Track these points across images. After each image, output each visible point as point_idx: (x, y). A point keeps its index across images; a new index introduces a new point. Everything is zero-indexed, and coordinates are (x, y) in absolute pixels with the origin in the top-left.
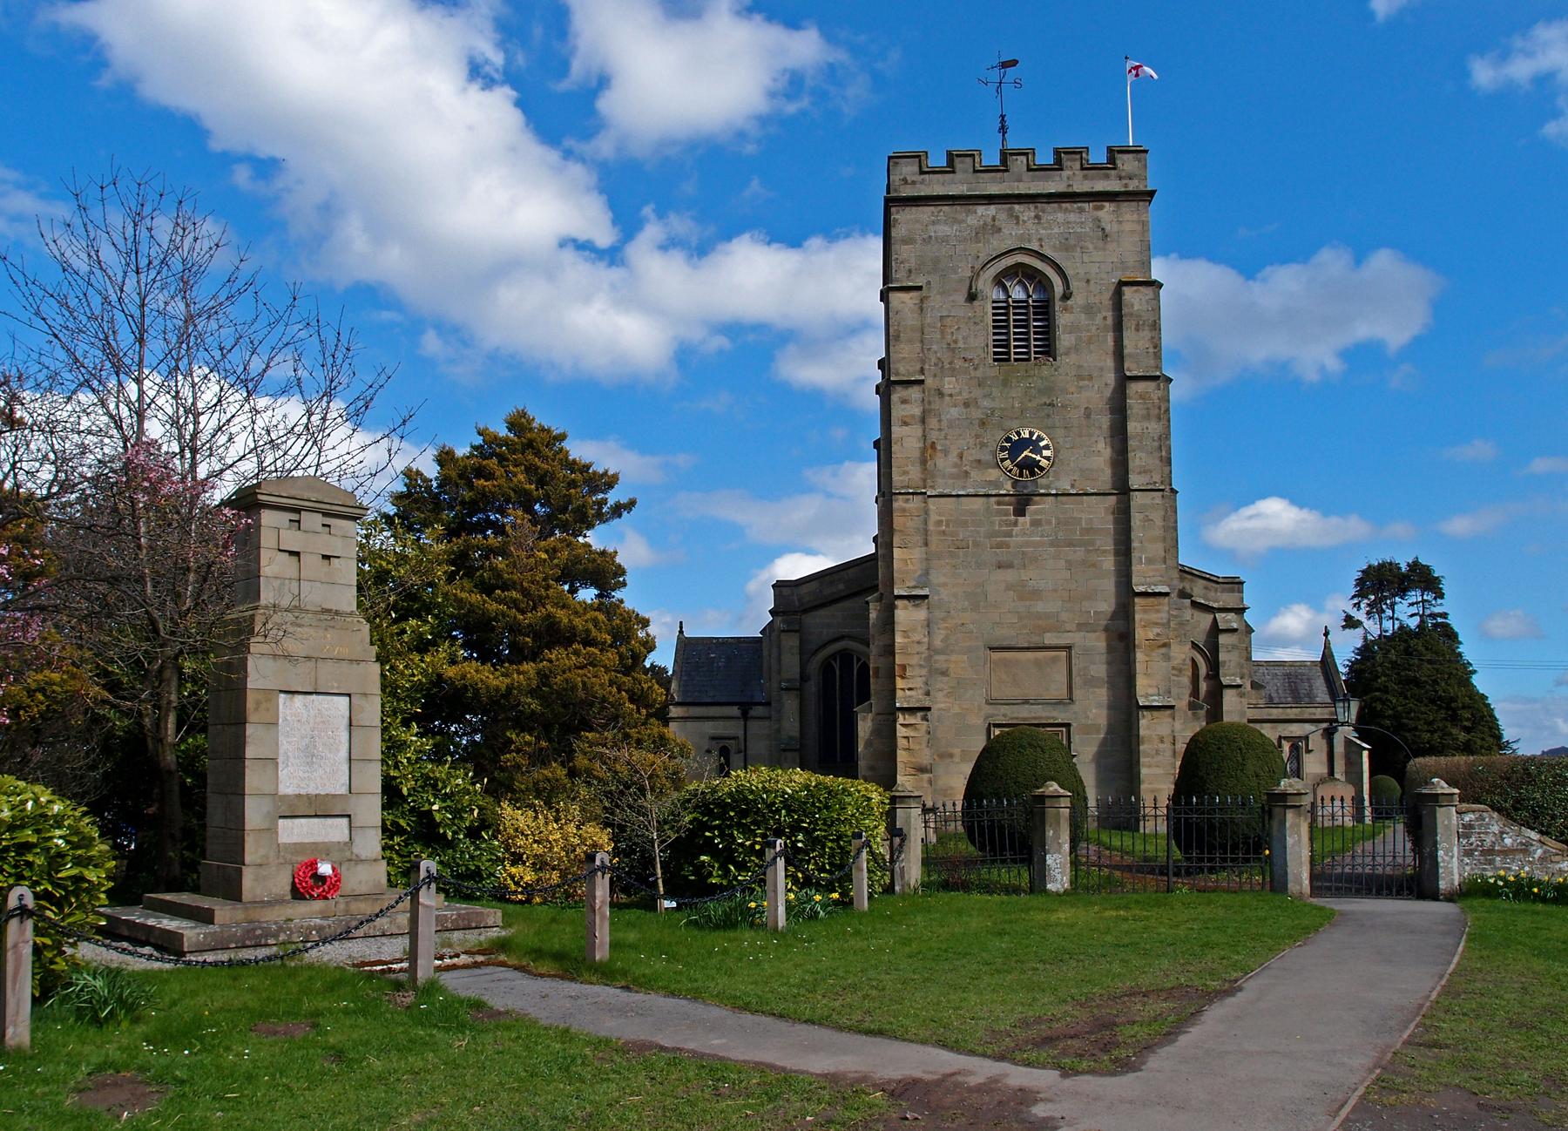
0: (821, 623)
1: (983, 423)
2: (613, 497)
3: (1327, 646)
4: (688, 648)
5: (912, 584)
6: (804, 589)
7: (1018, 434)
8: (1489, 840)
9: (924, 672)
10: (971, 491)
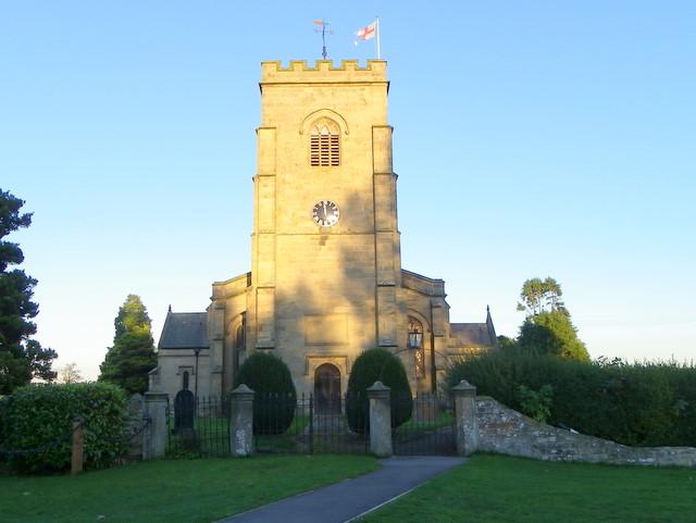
4: (173, 321)
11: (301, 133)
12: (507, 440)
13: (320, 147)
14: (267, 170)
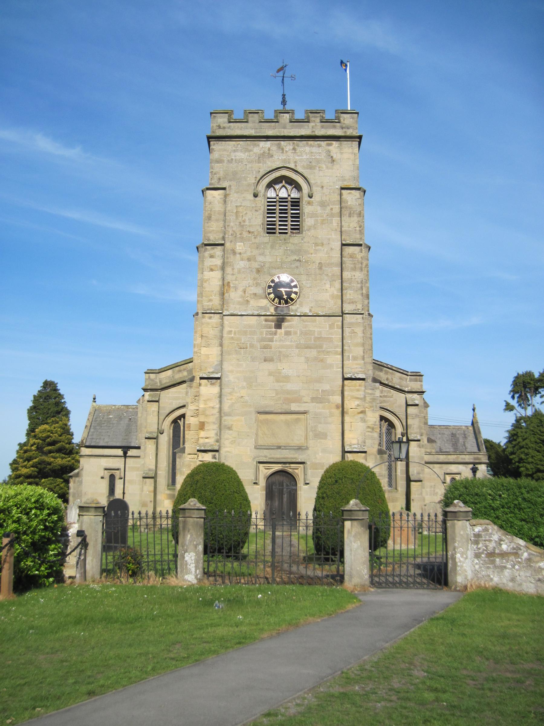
1: (258, 271)
8: (492, 545)
11: (256, 196)
12: (507, 572)
13: (278, 211)
14: (214, 238)
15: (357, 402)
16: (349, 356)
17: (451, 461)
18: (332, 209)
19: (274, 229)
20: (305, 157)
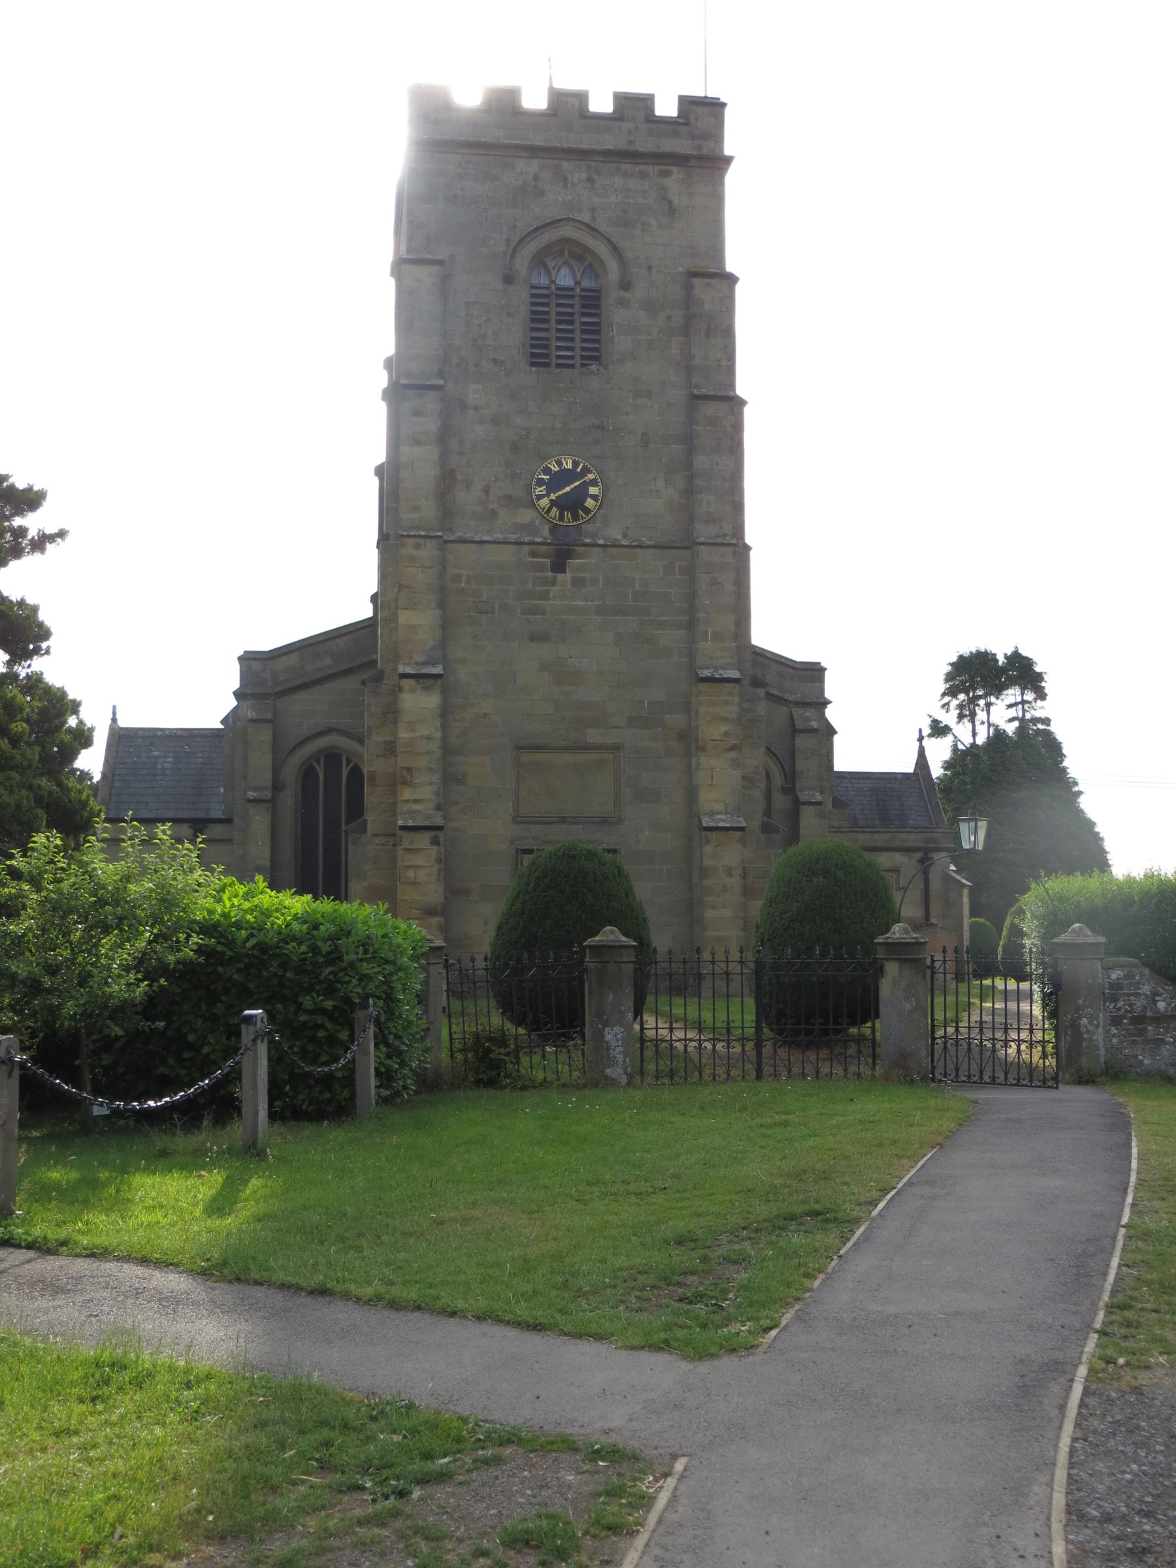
0: (307, 712)
1: (515, 448)
2: (33, 523)
3: (922, 751)
5: (421, 659)
6: (280, 664)
7: (559, 463)
8: (1139, 1004)
9: (435, 778)
10: (499, 536)
12: (1166, 1050)
15: (724, 728)
16: (706, 632)
17: (881, 844)
18: (669, 318)
19: (547, 356)
20: (613, 199)
